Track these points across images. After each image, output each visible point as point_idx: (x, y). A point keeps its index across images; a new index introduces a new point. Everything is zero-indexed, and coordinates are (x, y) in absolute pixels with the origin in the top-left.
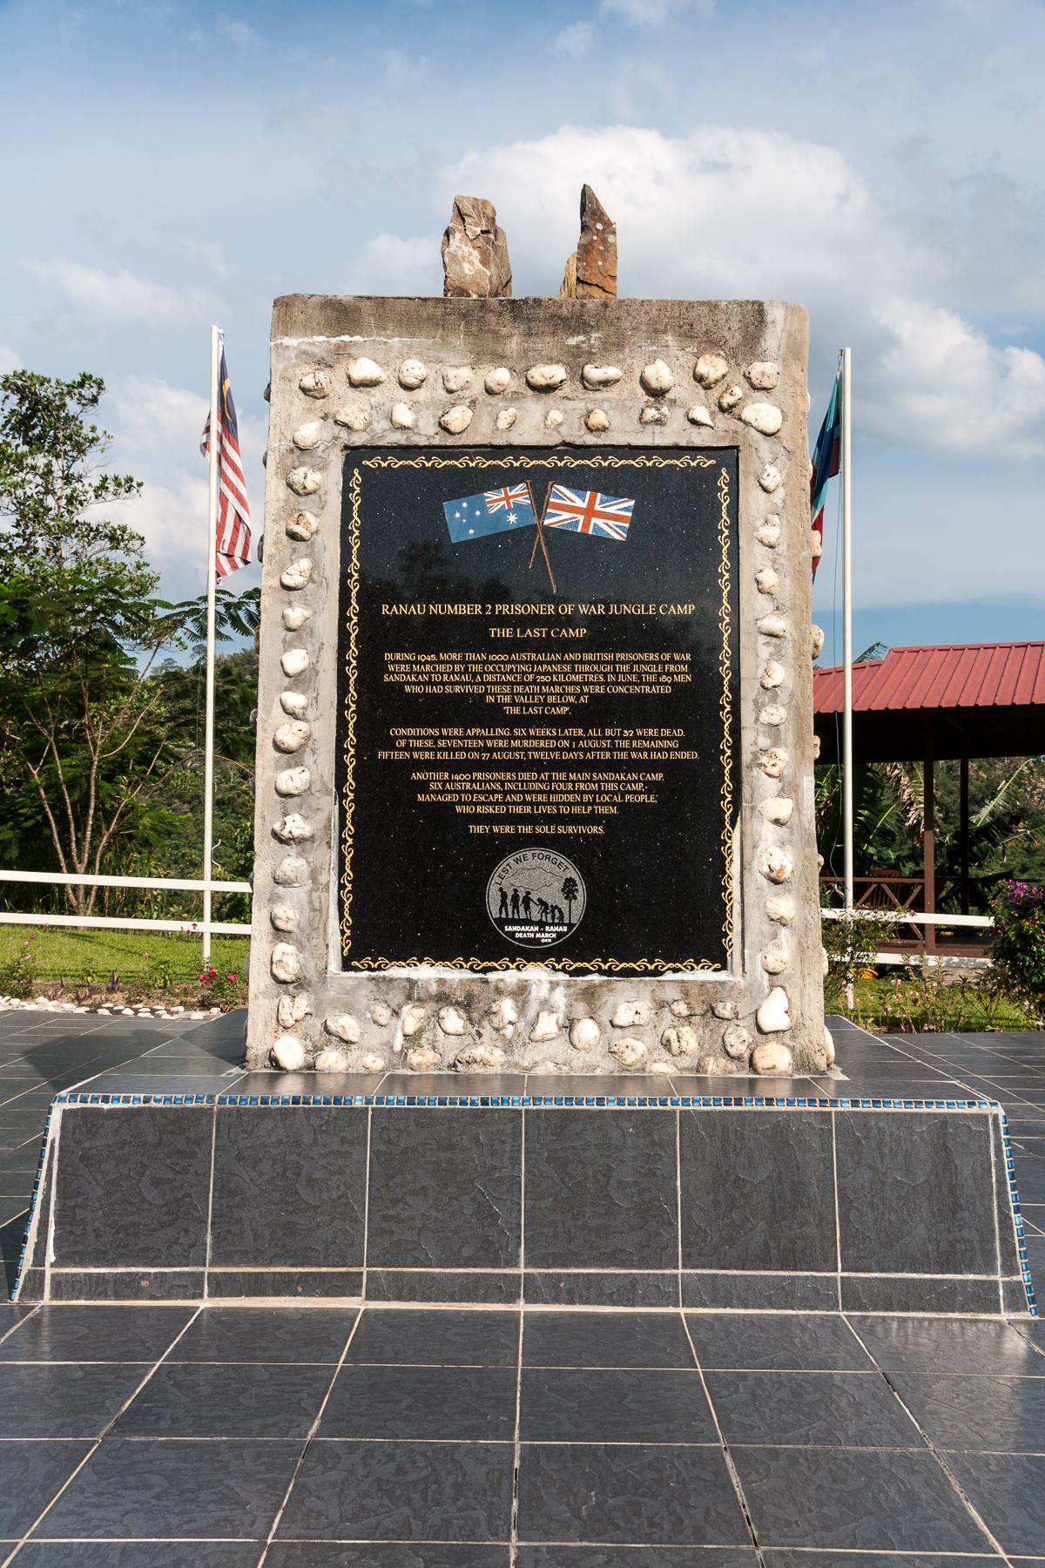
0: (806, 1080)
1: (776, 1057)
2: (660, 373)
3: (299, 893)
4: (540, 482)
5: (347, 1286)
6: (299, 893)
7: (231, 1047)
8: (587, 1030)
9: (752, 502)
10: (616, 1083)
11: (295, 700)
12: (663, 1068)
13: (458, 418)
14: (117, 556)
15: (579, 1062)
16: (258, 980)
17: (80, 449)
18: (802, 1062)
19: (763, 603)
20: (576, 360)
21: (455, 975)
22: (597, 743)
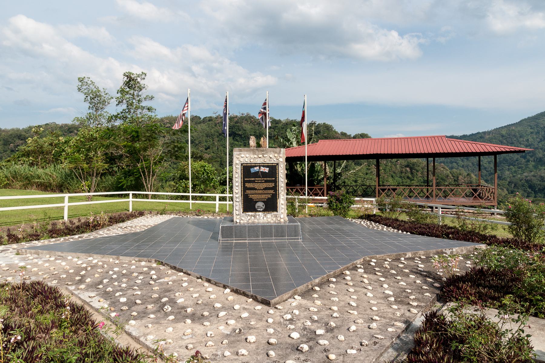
0: (285, 222)
1: (282, 220)
2: (271, 156)
3: (238, 206)
4: (260, 166)
5: (246, 240)
6: (238, 206)
7: (232, 221)
8: (265, 218)
9: (280, 168)
10: (268, 223)
11: (237, 188)
12: (272, 221)
13: (252, 160)
14: (150, 114)
15: (264, 221)
16: (234, 214)
17: (141, 90)
18: (285, 221)
19: (281, 178)
20: (263, 155)
21: (253, 213)
22: (266, 192)
